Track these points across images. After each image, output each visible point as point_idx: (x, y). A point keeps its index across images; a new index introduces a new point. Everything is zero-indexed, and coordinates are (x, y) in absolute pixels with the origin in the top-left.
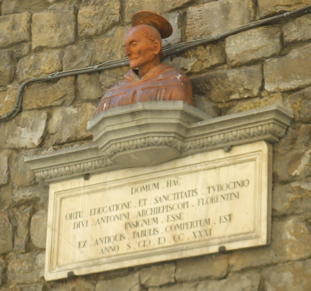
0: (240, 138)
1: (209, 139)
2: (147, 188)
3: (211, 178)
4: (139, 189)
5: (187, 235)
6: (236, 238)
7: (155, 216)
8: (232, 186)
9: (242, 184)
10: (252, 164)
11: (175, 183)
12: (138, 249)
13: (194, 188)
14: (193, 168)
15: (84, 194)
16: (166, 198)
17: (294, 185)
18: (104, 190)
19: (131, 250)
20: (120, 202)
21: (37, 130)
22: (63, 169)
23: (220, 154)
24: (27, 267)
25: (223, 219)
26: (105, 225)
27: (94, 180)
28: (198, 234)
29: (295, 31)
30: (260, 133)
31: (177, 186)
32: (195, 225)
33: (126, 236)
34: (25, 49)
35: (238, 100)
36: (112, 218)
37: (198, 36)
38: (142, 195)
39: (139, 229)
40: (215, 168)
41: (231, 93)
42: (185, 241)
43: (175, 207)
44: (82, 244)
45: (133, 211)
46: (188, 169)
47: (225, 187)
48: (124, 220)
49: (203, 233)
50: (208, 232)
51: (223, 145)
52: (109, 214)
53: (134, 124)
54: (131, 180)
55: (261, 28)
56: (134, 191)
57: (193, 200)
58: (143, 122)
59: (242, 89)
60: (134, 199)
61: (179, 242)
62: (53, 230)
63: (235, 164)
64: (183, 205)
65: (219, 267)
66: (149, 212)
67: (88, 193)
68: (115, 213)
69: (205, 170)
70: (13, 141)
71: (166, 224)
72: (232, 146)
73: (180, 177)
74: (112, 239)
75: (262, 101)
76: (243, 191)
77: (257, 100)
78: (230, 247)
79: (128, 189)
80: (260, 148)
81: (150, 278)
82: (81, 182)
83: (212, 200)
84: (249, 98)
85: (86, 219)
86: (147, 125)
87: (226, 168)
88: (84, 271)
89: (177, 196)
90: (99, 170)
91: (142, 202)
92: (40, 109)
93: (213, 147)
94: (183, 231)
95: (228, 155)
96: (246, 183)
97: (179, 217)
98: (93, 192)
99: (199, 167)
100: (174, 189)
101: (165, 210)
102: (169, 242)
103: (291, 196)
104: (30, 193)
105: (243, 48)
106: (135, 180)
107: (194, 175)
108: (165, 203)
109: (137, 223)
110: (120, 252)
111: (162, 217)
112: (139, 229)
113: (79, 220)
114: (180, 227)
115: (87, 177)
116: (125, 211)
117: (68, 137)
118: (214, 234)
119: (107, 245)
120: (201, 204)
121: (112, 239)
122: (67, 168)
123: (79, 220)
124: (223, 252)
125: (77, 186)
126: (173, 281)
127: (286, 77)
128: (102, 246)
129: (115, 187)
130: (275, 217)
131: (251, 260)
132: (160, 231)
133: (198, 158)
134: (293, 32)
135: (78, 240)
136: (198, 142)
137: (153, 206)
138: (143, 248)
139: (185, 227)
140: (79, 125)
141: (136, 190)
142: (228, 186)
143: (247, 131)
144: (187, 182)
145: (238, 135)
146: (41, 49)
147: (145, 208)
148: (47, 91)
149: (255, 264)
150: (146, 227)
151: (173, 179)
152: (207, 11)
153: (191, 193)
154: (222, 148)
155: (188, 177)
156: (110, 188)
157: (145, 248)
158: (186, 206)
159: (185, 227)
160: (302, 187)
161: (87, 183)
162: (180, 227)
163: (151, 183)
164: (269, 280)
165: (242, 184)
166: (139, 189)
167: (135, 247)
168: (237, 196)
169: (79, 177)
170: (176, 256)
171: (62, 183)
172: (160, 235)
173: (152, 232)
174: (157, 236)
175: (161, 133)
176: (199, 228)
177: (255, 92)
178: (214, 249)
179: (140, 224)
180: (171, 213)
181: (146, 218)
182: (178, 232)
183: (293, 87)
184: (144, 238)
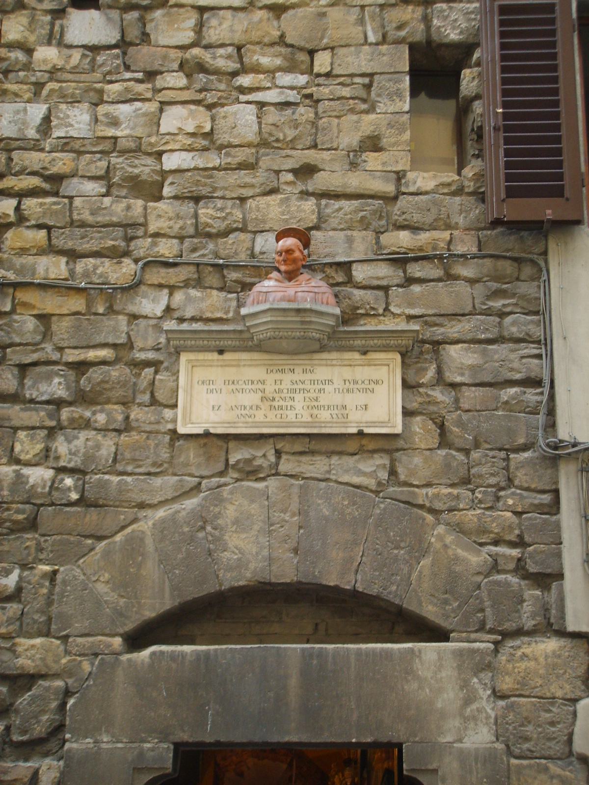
0: (379, 346)
1: (351, 342)
2: (283, 371)
3: (347, 373)
4: (274, 371)
5: (325, 415)
6: (373, 424)
7: (292, 395)
8: (367, 382)
9: (377, 382)
10: (386, 368)
11: (311, 372)
12: (274, 419)
13: (330, 379)
14: (329, 362)
15: (217, 366)
16: (303, 383)
17: (421, 390)
18: (238, 366)
19: (268, 420)
20: (255, 379)
21: (159, 303)
22: (201, 342)
23: (356, 356)
24: (152, 419)
25: (359, 408)
26: (240, 396)
27: (227, 356)
28: (335, 416)
29: (418, 271)
30: (398, 346)
31: (313, 375)
32: (332, 407)
33: (262, 407)
34: (140, 233)
35: (363, 315)
36: (248, 391)
37: (322, 256)
38: (278, 376)
39: (276, 404)
40: (350, 365)
41: (358, 308)
42: (322, 420)
43: (312, 391)
44: (216, 408)
45: (270, 388)
46: (324, 362)
47: (360, 382)
48: (260, 394)
49: (340, 416)
50: (345, 416)
51: (361, 349)
52: (244, 386)
53: (298, 319)
54: (266, 362)
55: (386, 262)
56: (269, 372)
57: (329, 388)
58: (308, 319)
59: (368, 306)
60: (271, 378)
61: (317, 420)
62: (185, 391)
63: (370, 365)
64: (320, 391)
65: (352, 446)
66: (285, 391)
67: (222, 366)
68: (250, 387)
69: (340, 365)
70: (132, 308)
71: (302, 404)
72: (367, 351)
73: (315, 367)
74: (248, 408)
75: (386, 319)
76: (377, 388)
77: (382, 318)
78: (367, 431)
79: (264, 369)
80: (395, 357)
81: (285, 445)
82: (215, 356)
83: (348, 390)
84: (374, 315)
85: (220, 387)
86: (310, 322)
87: (361, 367)
88: (220, 431)
89: (313, 382)
90: (235, 349)
91: (278, 382)
92: (161, 286)
93: (351, 349)
94: (319, 412)
95: (363, 357)
96: (380, 382)
97: (317, 400)
98: (226, 366)
99: (334, 362)
100: (308, 376)
101: (302, 392)
102: (306, 418)
103: (420, 399)
104: (153, 356)
105: (370, 274)
106: (271, 362)
107: (330, 368)
108: (301, 386)
109: (274, 399)
110: (257, 419)
111: (299, 397)
112: (276, 404)
113: (211, 387)
114: (318, 408)
115: (221, 352)
116: (260, 386)
117: (192, 315)
118: (350, 418)
119: (243, 412)
120: (337, 391)
121: (248, 408)
122: (206, 342)
123: (211, 387)
124: (361, 434)
125: (210, 358)
126: (307, 450)
127: (411, 305)
128: (239, 412)
129: (250, 365)
130: (407, 413)
131: (381, 444)
132: (297, 408)
133: (334, 355)
134: (416, 270)
135: (212, 403)
136: (340, 343)
137: (289, 387)
138: (280, 420)
139: (322, 409)
140: (204, 307)
141: (272, 371)
142: (363, 382)
143: (388, 342)
144: (322, 373)
145: (379, 344)
146: (156, 235)
147: (282, 387)
148: (202, 275)
149: (387, 447)
150: (282, 403)
151: (308, 368)
152: (331, 237)
153: (327, 382)
154: (359, 351)
155: (324, 368)
156: (244, 365)
157: (282, 420)
158: (322, 392)
159: (322, 409)
160: (429, 392)
161: (221, 357)
162: (318, 408)
163: (287, 367)
164: (400, 462)
165: (377, 382)
166: (274, 371)
167: (271, 416)
168: (373, 391)
169: (213, 351)
170: (315, 431)
171: (194, 353)
172: (297, 411)
173: (289, 408)
174: (295, 412)
175: (319, 330)
176: (336, 411)
177: (381, 311)
178: (354, 430)
179: (276, 400)
180: (307, 395)
181: (283, 395)
182: (315, 412)
183: (417, 314)
184: (281, 412)
